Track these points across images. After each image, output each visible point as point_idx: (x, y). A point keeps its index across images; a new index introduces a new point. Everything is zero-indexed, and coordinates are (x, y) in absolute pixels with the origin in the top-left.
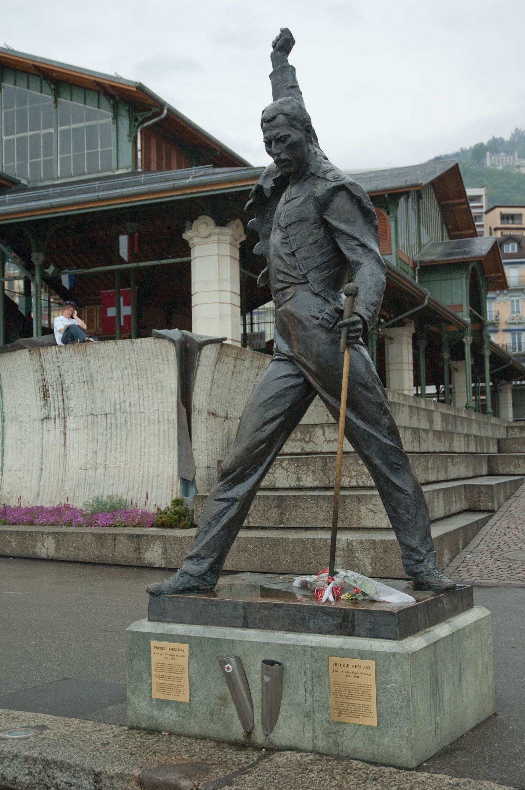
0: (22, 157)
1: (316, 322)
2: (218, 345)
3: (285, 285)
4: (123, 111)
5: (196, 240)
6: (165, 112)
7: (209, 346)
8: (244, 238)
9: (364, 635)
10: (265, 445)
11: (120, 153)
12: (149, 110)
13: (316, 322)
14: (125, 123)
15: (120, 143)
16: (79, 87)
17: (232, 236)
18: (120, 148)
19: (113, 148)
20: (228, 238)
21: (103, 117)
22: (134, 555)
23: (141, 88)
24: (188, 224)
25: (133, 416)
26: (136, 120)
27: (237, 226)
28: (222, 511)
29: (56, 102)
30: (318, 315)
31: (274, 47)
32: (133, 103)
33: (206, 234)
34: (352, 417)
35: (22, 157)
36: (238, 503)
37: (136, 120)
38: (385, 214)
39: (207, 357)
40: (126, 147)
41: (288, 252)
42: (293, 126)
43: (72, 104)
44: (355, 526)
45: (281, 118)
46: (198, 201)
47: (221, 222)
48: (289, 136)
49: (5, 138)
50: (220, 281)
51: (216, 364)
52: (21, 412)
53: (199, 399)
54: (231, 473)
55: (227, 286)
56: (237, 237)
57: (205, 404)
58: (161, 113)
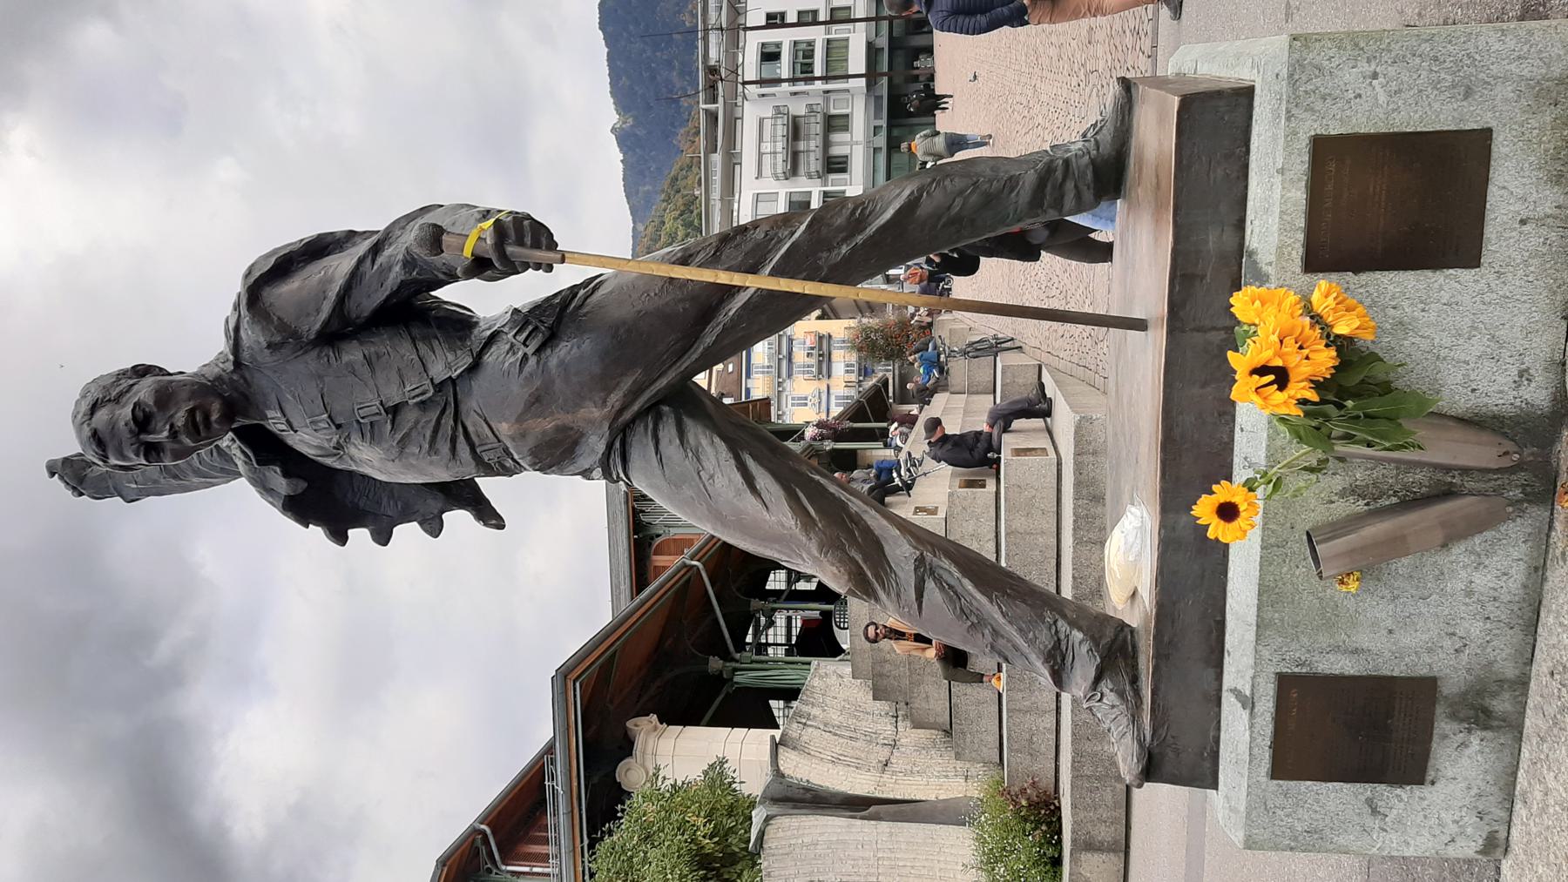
1: (532, 361)
2: (781, 749)
3: (461, 438)
7: (781, 762)
9: (1229, 237)
10: (801, 495)
12: (477, 852)
13: (532, 361)
28: (942, 589)
30: (520, 354)
31: (81, 494)
34: (741, 299)
36: (928, 556)
38: (658, 541)
39: (797, 768)
41: (389, 427)
46: (595, 780)
47: (626, 747)
53: (860, 784)
54: (861, 573)
58: (483, 833)
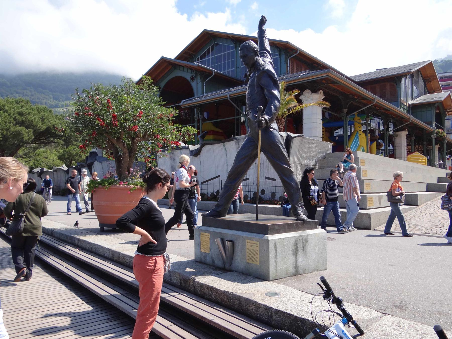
4: (283, 53)
6: (214, 74)
14: (283, 57)
23: (287, 43)
37: (287, 55)
47: (314, 91)
49: (241, 67)
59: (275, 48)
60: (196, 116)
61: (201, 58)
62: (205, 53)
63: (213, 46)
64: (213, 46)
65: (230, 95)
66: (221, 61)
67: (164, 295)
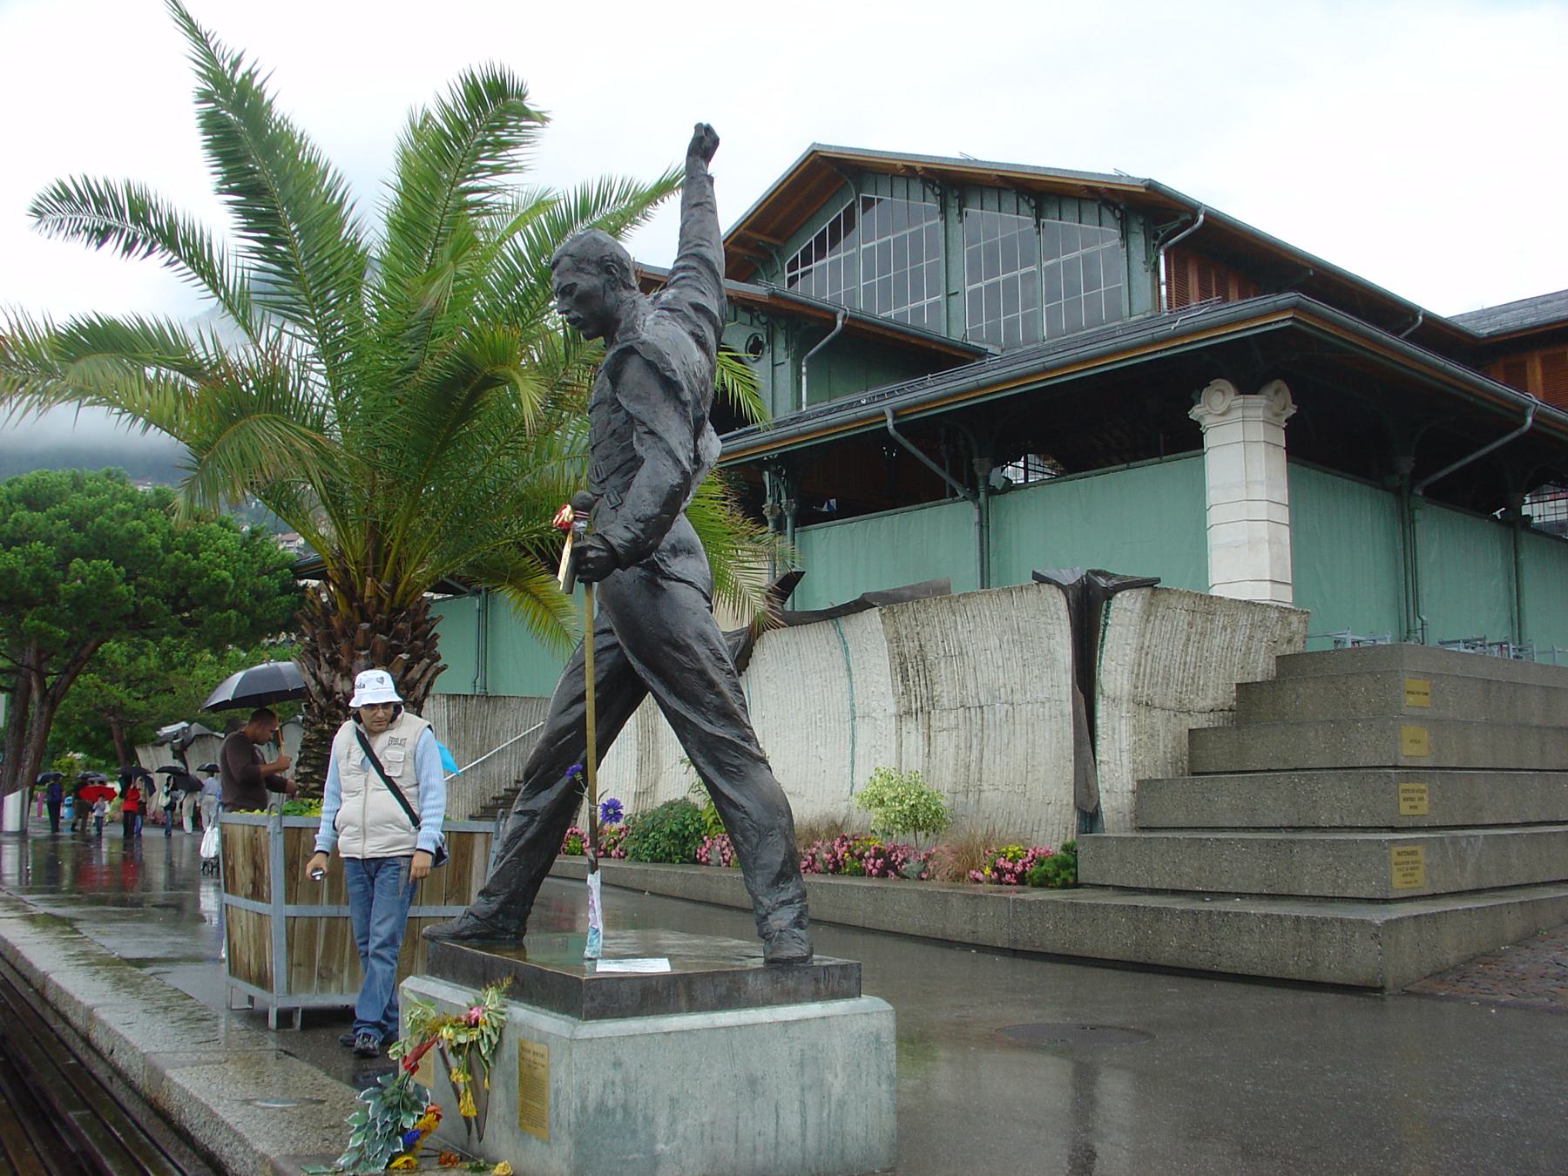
0: (993, 314)
2: (1146, 591)
4: (1136, 227)
5: (1206, 422)
6: (1201, 217)
8: (1292, 411)
11: (1134, 290)
14: (1138, 242)
15: (1134, 276)
16: (1073, 197)
17: (1267, 408)
18: (1133, 284)
19: (1123, 284)
20: (1260, 412)
21: (1100, 239)
22: (968, 927)
23: (1152, 187)
24: (1194, 396)
25: (1017, 709)
26: (1156, 237)
27: (1276, 392)
29: (1038, 225)
32: (1147, 211)
33: (1222, 408)
35: (993, 314)
37: (1156, 237)
40: (1143, 279)
42: (581, 270)
43: (1062, 223)
44: (1307, 892)
45: (566, 261)
47: (1247, 386)
48: (575, 284)
49: (968, 288)
50: (1248, 484)
51: (1148, 621)
52: (875, 703)
55: (1260, 492)
56: (1277, 410)
57: (1127, 687)
58: (1195, 220)
59: (1104, 210)
60: (769, 501)
61: (806, 260)
62: (820, 239)
63: (852, 207)
64: (852, 207)
65: (896, 414)
66: (884, 270)
67: (474, 897)
